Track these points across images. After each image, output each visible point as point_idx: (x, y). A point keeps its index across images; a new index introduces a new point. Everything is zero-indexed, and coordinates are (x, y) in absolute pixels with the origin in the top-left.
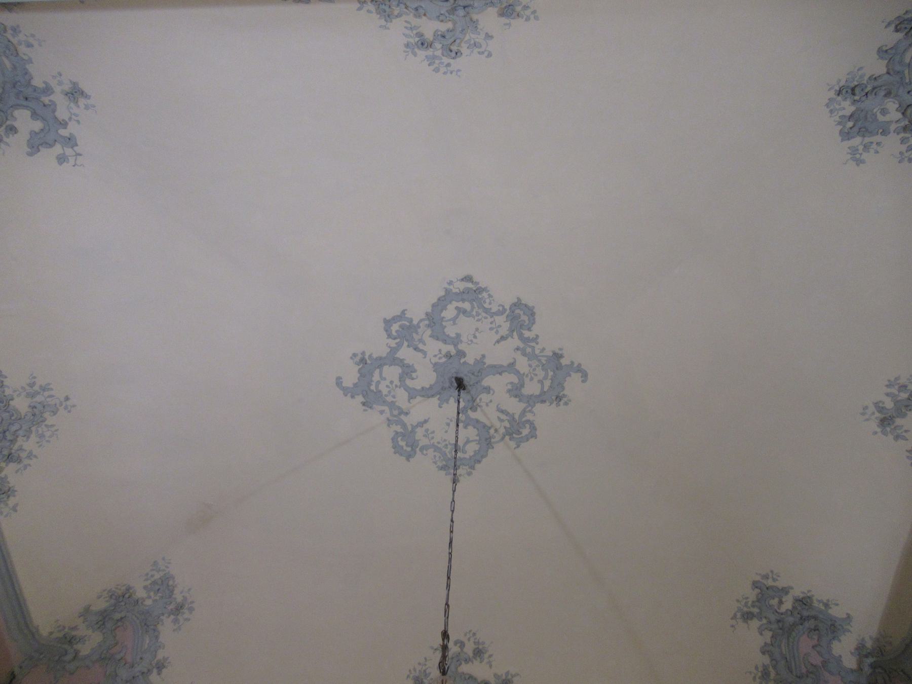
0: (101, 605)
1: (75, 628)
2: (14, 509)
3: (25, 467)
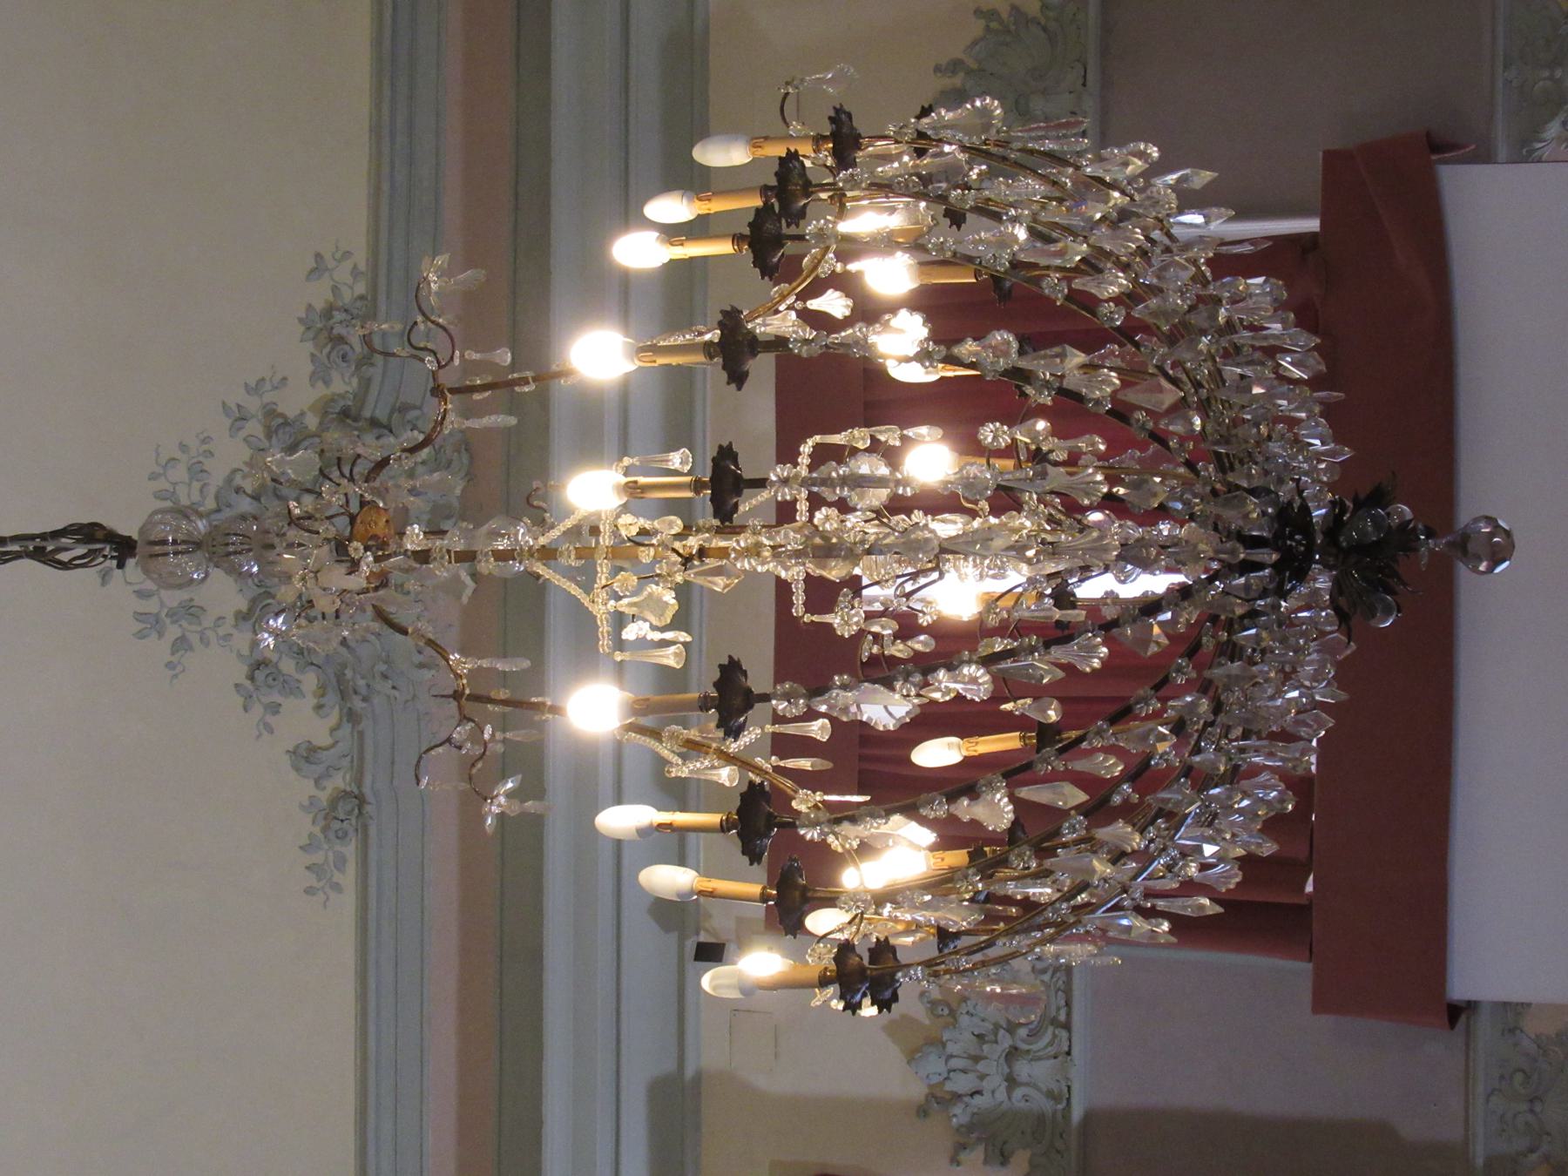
2: (319, 268)
3: (255, 389)
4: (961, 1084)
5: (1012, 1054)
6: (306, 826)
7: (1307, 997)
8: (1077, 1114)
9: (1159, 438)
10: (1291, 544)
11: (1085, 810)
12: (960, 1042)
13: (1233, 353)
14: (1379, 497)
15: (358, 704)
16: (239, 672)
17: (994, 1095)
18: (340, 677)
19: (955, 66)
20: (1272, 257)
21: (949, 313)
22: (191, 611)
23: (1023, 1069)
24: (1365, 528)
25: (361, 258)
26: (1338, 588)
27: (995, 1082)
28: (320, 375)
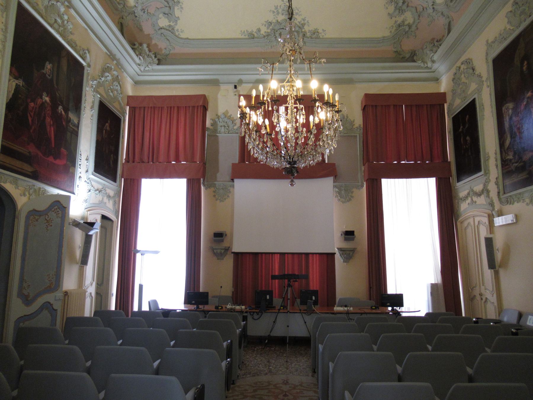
0: (391, 9)
1: (396, 22)
2: (324, 31)
3: (308, 22)
4: (221, 120)
5: (225, 126)
6: (250, 30)
7: (234, 162)
8: (218, 135)
9: (304, 148)
10: (292, 163)
11: (263, 141)
12: (226, 120)
13: (313, 156)
14: (297, 172)
15: (266, 38)
16: (270, 21)
17: (220, 124)
18: (269, 35)
19: (347, 117)
20: (323, 160)
21: (319, 127)
22: (278, 13)
23: (223, 128)
24: (294, 171)
25: (325, 37)
26: (288, 168)
27: (221, 124)
28: (310, 31)
